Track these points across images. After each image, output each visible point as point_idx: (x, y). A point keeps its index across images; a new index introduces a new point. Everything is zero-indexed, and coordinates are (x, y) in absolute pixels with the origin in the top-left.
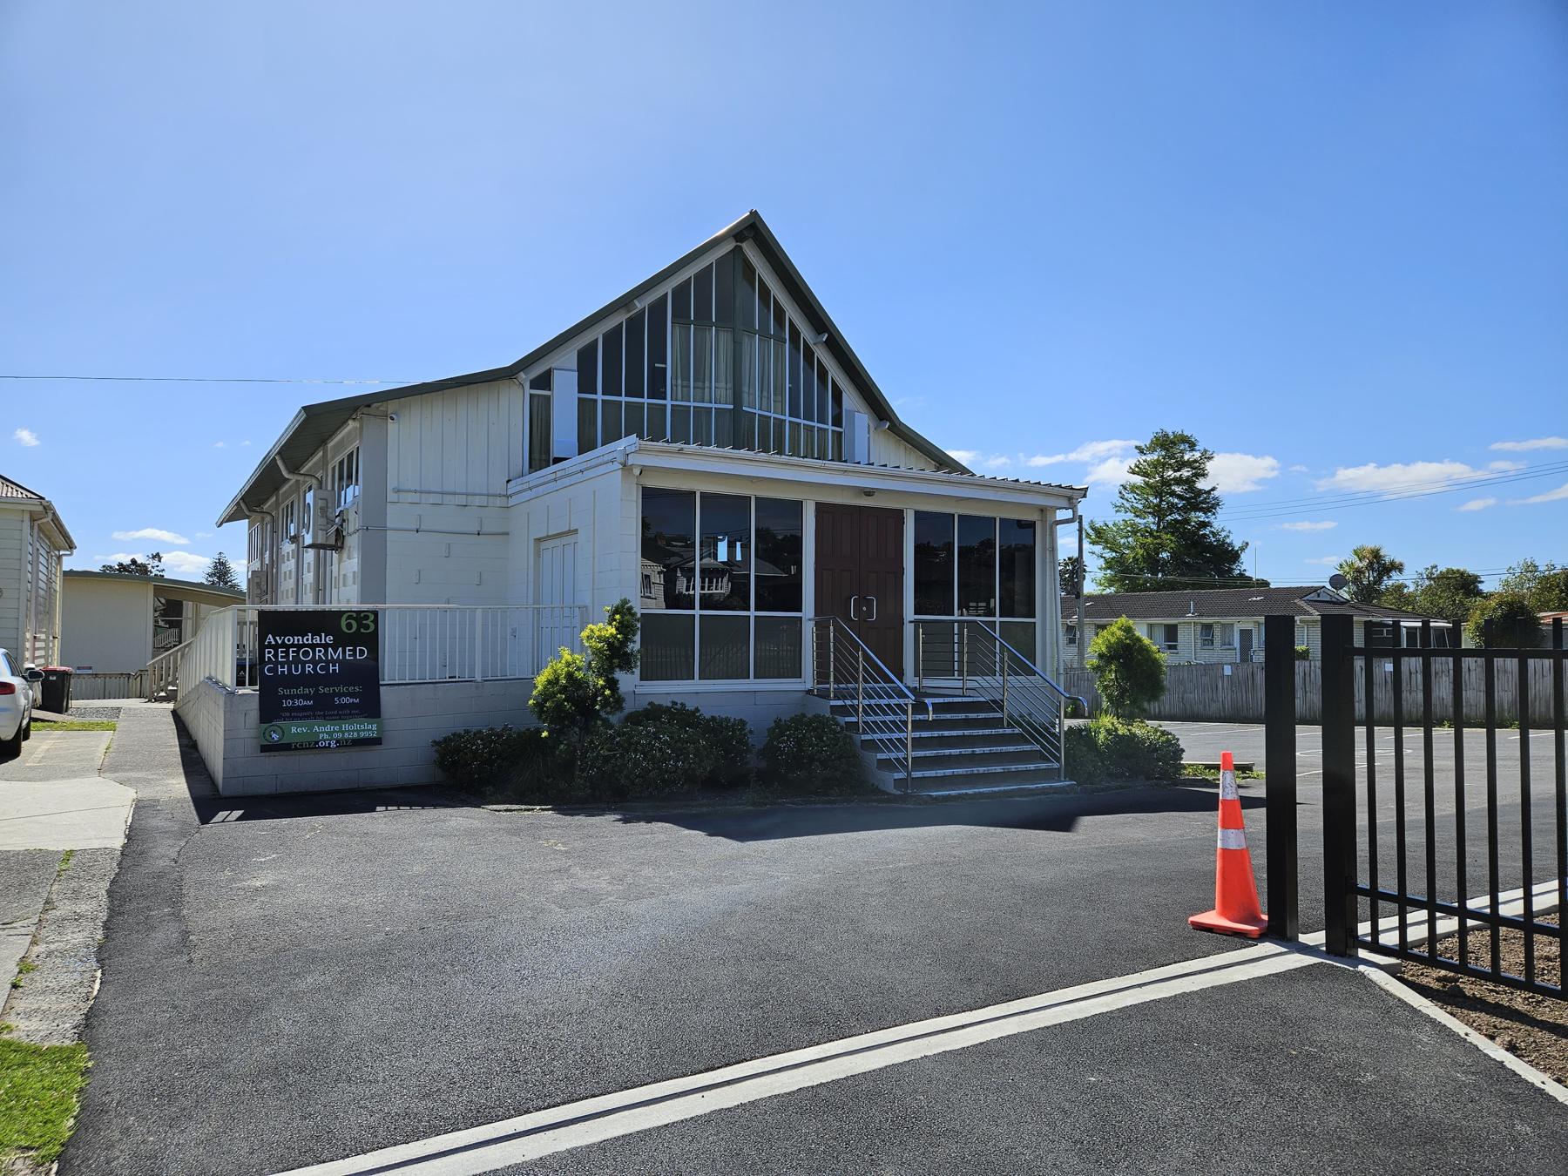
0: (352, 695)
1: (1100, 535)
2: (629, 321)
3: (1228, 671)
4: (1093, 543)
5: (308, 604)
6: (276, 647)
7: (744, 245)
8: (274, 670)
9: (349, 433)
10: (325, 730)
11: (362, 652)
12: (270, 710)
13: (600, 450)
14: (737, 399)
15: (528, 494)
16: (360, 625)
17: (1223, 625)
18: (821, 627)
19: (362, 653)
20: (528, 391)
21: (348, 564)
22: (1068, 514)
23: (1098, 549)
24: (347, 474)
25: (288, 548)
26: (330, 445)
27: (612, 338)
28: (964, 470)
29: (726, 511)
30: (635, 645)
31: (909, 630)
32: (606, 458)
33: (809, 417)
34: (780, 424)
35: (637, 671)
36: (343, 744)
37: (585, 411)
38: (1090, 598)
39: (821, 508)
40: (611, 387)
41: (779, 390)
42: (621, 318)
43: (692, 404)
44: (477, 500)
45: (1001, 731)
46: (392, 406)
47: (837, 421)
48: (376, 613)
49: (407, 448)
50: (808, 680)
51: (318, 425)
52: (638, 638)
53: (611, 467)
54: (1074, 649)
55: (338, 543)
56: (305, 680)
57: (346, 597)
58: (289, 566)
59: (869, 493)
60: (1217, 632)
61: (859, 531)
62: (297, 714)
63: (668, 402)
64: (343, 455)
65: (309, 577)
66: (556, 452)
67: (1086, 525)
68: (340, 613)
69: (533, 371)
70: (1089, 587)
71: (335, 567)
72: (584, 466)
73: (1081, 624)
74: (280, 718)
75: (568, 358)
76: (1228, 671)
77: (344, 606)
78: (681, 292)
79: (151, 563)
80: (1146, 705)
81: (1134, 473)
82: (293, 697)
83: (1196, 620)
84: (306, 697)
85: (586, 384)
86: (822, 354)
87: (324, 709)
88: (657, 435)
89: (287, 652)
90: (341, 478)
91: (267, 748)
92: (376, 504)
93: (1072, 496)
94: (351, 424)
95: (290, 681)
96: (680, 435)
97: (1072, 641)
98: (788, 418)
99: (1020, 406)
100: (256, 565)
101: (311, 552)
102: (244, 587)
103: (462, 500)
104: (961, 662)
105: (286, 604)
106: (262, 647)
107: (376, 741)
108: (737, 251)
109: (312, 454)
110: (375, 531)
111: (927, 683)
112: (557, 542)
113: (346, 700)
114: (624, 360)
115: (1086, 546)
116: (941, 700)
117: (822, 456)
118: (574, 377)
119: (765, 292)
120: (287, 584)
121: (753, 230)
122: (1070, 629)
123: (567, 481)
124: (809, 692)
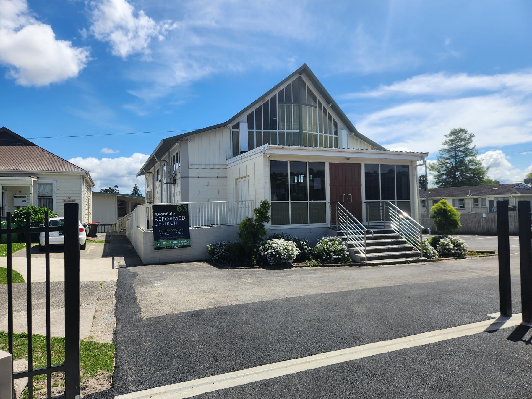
0: (181, 231)
1: (432, 168)
2: (264, 105)
3: (484, 215)
4: (430, 170)
5: (165, 203)
6: (158, 217)
7: (302, 76)
8: (157, 224)
9: (176, 147)
10: (173, 243)
11: (184, 218)
12: (157, 236)
13: (256, 149)
14: (301, 129)
15: (233, 164)
16: (183, 209)
17: (482, 199)
18: (333, 206)
19: (183, 218)
20: (232, 130)
21: (177, 189)
22: (422, 162)
23: (432, 172)
24: (176, 159)
25: (158, 183)
26: (171, 150)
27: (258, 111)
28: (385, 150)
29: (298, 167)
30: (269, 214)
31: (364, 206)
32: (258, 151)
33: (325, 133)
34: (316, 136)
35: (270, 222)
36: (179, 247)
37: (250, 135)
38: (431, 190)
39: (331, 165)
40: (258, 127)
41: (315, 124)
42: (261, 104)
43: (286, 131)
44: (217, 167)
45: (328, 206)
46: (189, 137)
47: (336, 133)
48: (187, 205)
49: (197, 153)
50: (328, 224)
51: (167, 145)
52: (270, 210)
53: (260, 154)
54: (425, 209)
55: (174, 182)
56: (167, 227)
57: (177, 200)
58: (158, 189)
59: (348, 159)
60: (480, 201)
61: (345, 171)
62: (165, 238)
63: (278, 131)
64: (175, 154)
65: (165, 193)
66: (241, 150)
67: (427, 165)
68: (177, 205)
69: (233, 124)
70: (431, 186)
71: (173, 190)
72: (251, 154)
73: (427, 200)
74: (160, 239)
75: (245, 117)
76: (484, 215)
77: (176, 203)
78: (281, 94)
79: (115, 188)
80: (452, 230)
81: (445, 144)
82: (163, 232)
83: (472, 197)
84: (167, 232)
85: (250, 126)
86: (329, 111)
87: (173, 236)
88: (274, 143)
89: (161, 218)
90: (174, 161)
91: (156, 249)
92: (185, 168)
93: (423, 156)
94: (177, 144)
95: (162, 227)
96: (282, 143)
97: (424, 206)
98: (318, 134)
99: (408, 125)
100: (148, 190)
101: (166, 185)
102: (144, 195)
103: (211, 167)
104: (383, 216)
105: (158, 203)
106: (154, 217)
107: (189, 246)
108: (300, 78)
109: (165, 153)
110: (185, 178)
111: (371, 224)
112: (243, 180)
113: (179, 233)
114: (265, 119)
115: (428, 170)
116: (376, 230)
117: (331, 147)
118: (246, 124)
119: (309, 91)
120: (158, 195)
121: (304, 70)
122: (423, 202)
123: (245, 159)
124: (329, 228)
